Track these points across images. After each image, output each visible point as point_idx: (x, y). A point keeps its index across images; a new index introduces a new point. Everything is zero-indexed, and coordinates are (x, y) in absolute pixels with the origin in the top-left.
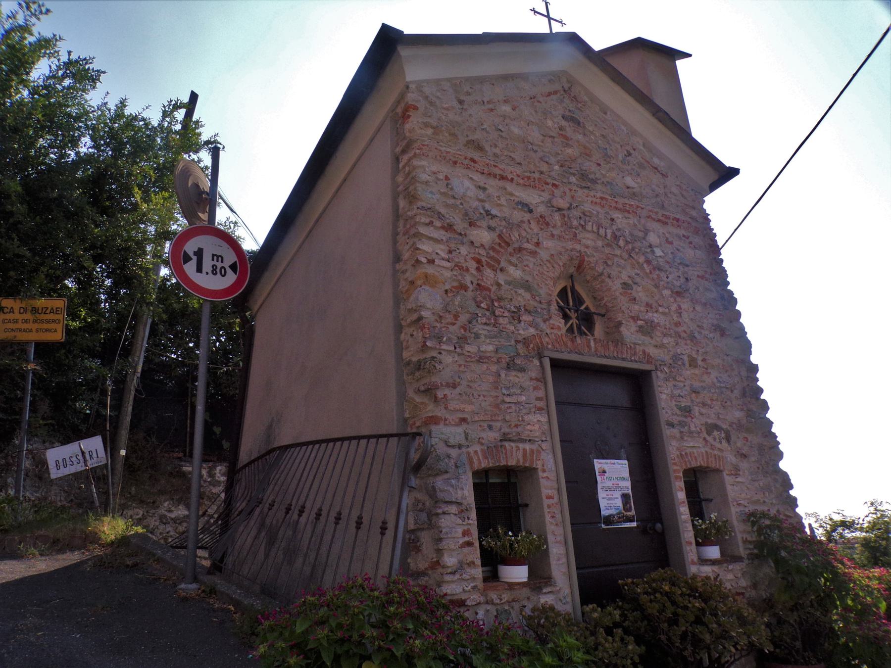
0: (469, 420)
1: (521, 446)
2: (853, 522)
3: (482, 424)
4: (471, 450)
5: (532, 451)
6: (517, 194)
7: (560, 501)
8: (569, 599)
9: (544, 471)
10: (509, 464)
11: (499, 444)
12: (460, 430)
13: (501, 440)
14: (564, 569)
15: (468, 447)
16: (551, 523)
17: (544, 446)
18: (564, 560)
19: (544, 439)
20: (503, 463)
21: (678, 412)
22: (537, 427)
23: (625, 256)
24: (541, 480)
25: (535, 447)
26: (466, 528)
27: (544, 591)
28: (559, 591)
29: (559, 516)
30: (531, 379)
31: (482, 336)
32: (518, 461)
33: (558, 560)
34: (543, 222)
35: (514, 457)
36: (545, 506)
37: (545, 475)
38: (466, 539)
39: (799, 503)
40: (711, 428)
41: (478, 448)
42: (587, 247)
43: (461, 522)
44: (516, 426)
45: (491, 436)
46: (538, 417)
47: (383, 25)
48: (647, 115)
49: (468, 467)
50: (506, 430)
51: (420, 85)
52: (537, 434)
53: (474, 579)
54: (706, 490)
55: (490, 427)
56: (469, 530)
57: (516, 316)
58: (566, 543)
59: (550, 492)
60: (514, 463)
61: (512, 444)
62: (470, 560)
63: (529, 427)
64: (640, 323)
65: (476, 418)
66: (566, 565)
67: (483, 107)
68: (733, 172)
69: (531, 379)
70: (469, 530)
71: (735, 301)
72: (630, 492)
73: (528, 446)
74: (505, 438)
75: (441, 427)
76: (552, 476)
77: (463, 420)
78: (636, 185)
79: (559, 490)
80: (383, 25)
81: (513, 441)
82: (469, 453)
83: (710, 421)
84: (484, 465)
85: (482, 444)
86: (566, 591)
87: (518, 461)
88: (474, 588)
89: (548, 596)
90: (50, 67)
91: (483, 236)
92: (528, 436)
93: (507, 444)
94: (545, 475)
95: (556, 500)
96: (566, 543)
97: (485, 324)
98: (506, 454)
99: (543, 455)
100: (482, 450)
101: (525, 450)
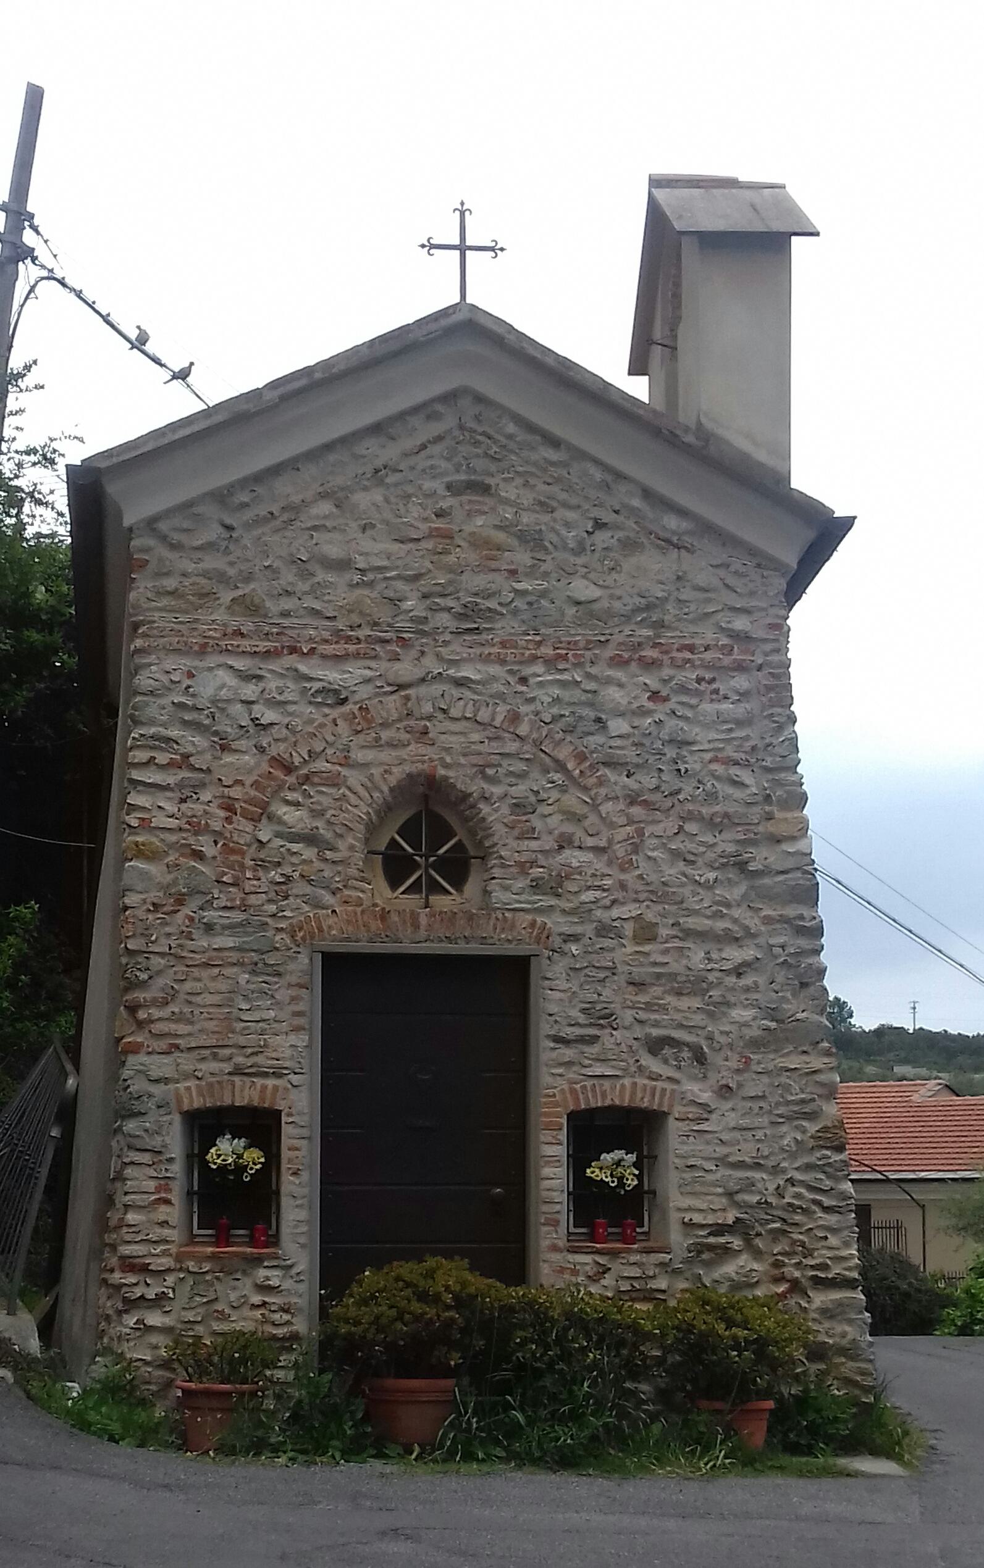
6: (319, 673)
9: (289, 1115)
13: (230, 1074)
20: (227, 1101)
21: (582, 1019)
23: (528, 750)
24: (547, 1079)
28: (291, 1267)
30: (290, 985)
31: (217, 927)
34: (364, 720)
39: (797, 714)
40: (655, 1046)
42: (448, 750)
46: (293, 1039)
47: (630, 374)
50: (240, 1060)
51: (151, 523)
54: (637, 979)
57: (282, 890)
64: (536, 872)
67: (277, 523)
68: (847, 524)
69: (290, 985)
71: (803, 799)
72: (300, 1107)
73: (270, 1082)
75: (142, 1058)
78: (597, 593)
80: (630, 374)
83: (655, 1032)
84: (197, 1103)
91: (244, 761)
93: (237, 1079)
97: (225, 908)
101: (264, 1088)
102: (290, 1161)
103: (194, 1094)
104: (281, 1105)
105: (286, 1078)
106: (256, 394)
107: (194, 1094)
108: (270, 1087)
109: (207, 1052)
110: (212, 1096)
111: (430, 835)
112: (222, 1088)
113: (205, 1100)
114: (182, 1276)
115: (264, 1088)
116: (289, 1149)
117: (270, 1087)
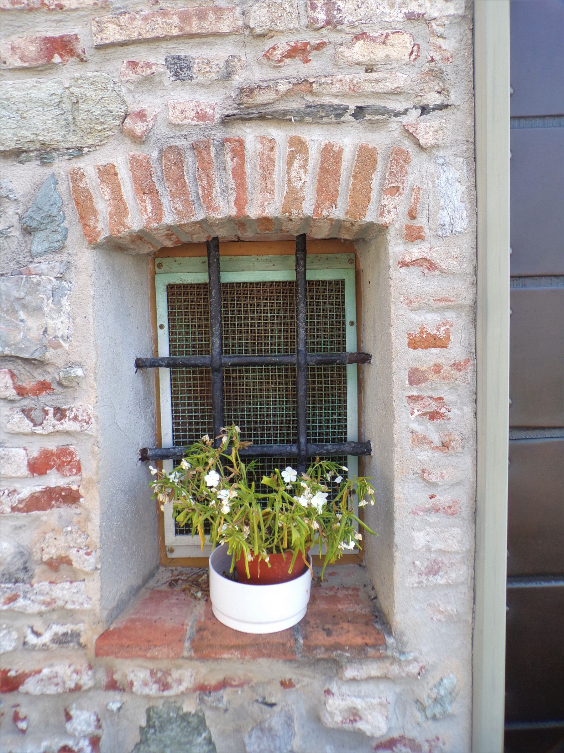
0: (85, 43)
1: (316, 137)
2: (211, 603)
3: (143, 55)
4: (88, 166)
5: (366, 158)
7: (475, 356)
8: (458, 708)
9: (413, 235)
10: (253, 212)
11: (218, 134)
12: (47, 87)
14: (455, 603)
15: (79, 152)
16: (421, 441)
17: (428, 129)
18: (459, 573)
19: (433, 99)
20: (225, 209)
22: (400, 47)
24: (397, 274)
25: (380, 140)
26: (52, 445)
27: (350, 673)
29: (459, 415)
32: (293, 198)
33: (434, 570)
35: (279, 181)
36: (400, 377)
37: (416, 251)
38: (54, 479)
41: (119, 156)
43: (27, 426)
44: (299, 51)
45: (175, 106)
48: (557, 430)
49: (75, 232)
50: (252, 73)
52: (401, 80)
53: (67, 614)
55: (180, 69)
56: (64, 452)
58: (476, 514)
59: (430, 321)
60: (273, 210)
61: (278, 134)
62: (52, 552)
63: (359, 51)
65: (113, 34)
66: (465, 590)
70: (64, 452)
73: (348, 139)
74: (247, 111)
76: (453, 256)
77: (62, 46)
79: (476, 313)
81: (280, 118)
82: (76, 177)
85: (140, 140)
86: (452, 676)
87: (293, 198)
88: (62, 640)
89: (365, 688)
90: (361, 472)
92: (354, 90)
93: (250, 135)
94: (416, 251)
95: (456, 351)
96: (476, 514)
98: (239, 174)
99: (419, 170)
100: (136, 164)
101: (331, 157)
102: (416, 377)
103: (128, 190)
104: (389, 212)
105: (394, 125)
106: (508, 613)
107: (128, 190)
108: (348, 158)
109: (157, 59)
110: (180, 190)
111: (333, 694)
112: (204, 166)
113: (158, 206)
114: (114, 706)
115: (331, 157)
116: (414, 344)
117: (348, 158)
